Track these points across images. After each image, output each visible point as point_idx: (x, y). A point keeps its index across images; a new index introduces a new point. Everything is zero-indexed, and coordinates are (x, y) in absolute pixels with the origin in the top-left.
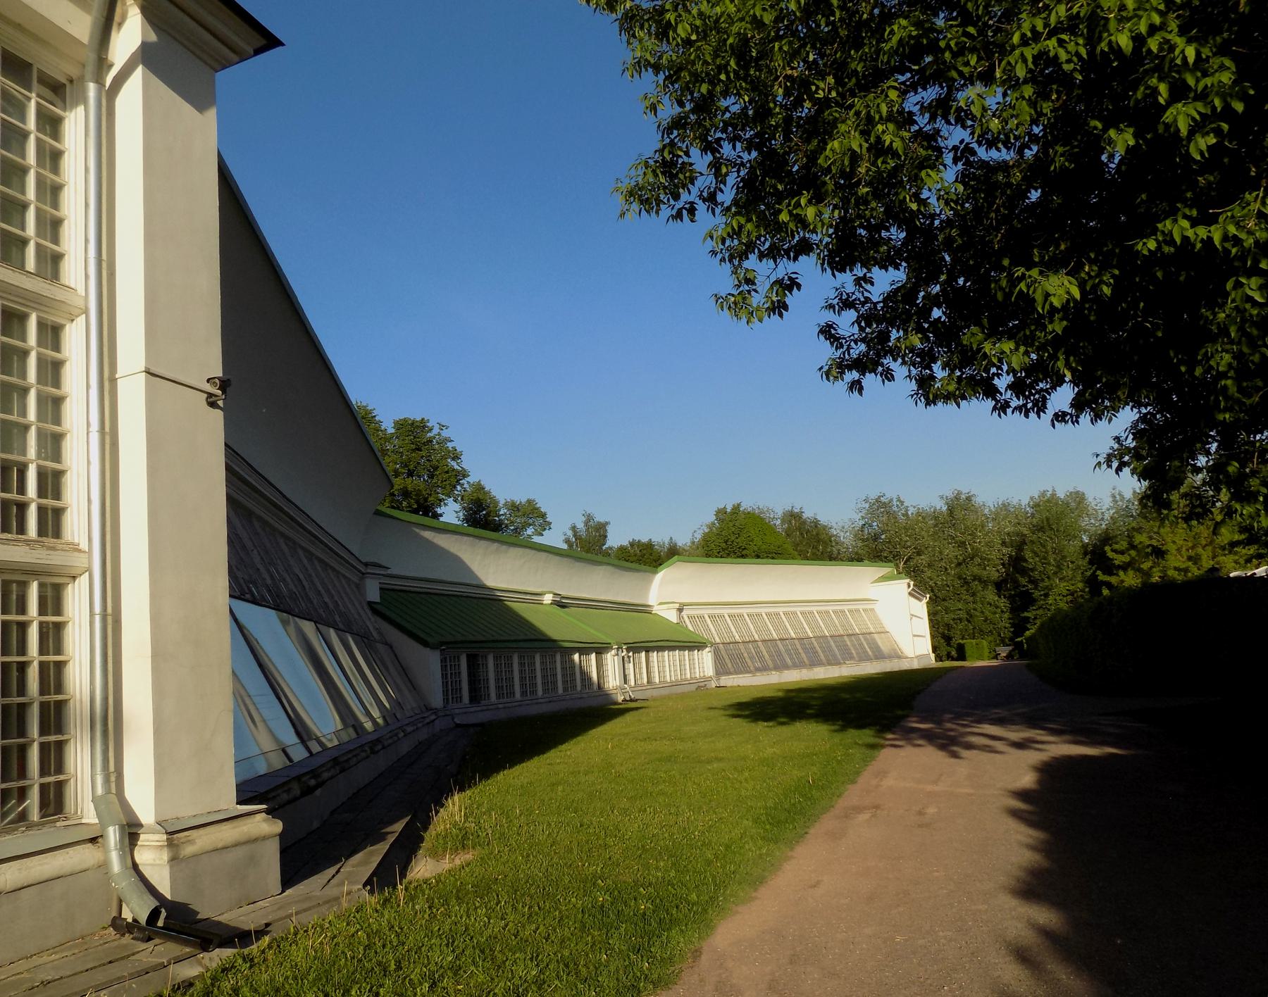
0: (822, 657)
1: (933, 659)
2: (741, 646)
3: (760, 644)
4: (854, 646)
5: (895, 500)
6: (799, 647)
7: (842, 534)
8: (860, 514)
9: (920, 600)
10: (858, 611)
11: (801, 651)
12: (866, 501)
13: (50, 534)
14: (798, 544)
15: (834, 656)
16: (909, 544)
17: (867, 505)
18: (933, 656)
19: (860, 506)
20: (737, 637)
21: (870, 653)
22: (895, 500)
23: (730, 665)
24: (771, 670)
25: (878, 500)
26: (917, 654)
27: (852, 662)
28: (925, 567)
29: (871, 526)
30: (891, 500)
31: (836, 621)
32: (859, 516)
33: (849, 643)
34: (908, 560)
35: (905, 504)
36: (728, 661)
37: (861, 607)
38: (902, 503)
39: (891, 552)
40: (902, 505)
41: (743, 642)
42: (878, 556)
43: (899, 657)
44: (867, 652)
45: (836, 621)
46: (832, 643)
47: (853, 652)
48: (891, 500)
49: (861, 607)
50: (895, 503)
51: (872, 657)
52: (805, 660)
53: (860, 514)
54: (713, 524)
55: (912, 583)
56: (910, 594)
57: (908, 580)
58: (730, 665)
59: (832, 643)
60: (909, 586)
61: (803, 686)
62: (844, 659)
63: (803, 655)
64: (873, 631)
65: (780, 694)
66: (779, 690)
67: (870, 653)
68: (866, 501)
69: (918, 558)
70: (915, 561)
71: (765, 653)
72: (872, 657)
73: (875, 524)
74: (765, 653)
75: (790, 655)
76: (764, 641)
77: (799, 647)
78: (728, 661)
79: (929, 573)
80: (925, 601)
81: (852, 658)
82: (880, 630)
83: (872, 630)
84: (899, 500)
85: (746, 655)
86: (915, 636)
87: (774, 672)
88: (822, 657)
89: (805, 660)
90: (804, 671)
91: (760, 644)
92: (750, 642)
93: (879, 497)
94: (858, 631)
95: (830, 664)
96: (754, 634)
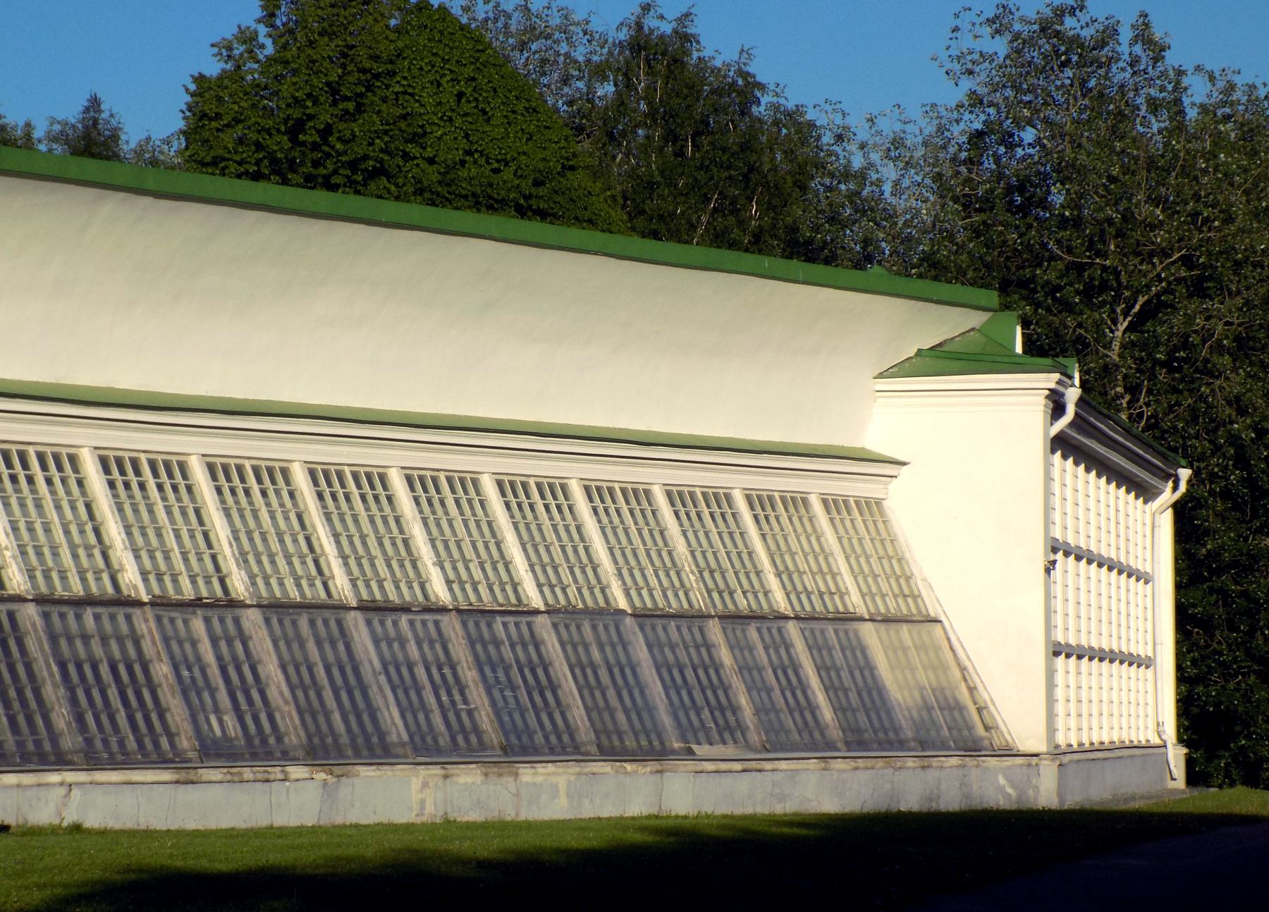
0: (578, 715)
1: (1179, 770)
2: (145, 624)
3: (252, 619)
4: (747, 669)
5: (1126, 34)
6: (460, 651)
7: (889, 172)
8: (967, 84)
9: (1145, 492)
10: (797, 502)
11: (469, 675)
12: (998, 24)
13: (1069, 431)
14: (651, 186)
15: (641, 710)
16: (1160, 237)
17: (1000, 47)
18: (1176, 756)
19: (966, 42)
20: (130, 577)
21: (827, 714)
22: (1126, 34)
23: (62, 717)
24: (287, 757)
25: (1046, 28)
26: (1067, 736)
27: (729, 750)
28: (1219, 348)
29: (1009, 141)
30: (1109, 34)
31: (681, 547)
32: (958, 93)
33: (725, 656)
34: (1149, 312)
35: (1172, 59)
36: (53, 693)
37: (815, 487)
38: (1158, 51)
39: (1080, 268)
40: (1156, 60)
41: (160, 603)
42: (1023, 284)
43: (972, 747)
44: (813, 709)
45: (681, 547)
46: (641, 653)
47: (743, 700)
48: (1109, 34)
49: (815, 487)
50: (1124, 49)
51: (835, 733)
52: (485, 719)
53: (967, 84)
54: (247, 38)
55: (1073, 394)
56: (1060, 444)
57: (1050, 380)
58: (62, 717)
59: (641, 653)
60: (1057, 409)
61: (273, 857)
62: (692, 733)
63: (478, 696)
64: (862, 611)
65: (648, 838)
66: (643, 829)
67: (827, 714)
68: (998, 24)
69: (1193, 305)
70: (1177, 320)
71: (271, 669)
72: (835, 733)
73: (1029, 135)
74: (271, 669)
75: (404, 687)
76: (275, 608)
77: (460, 651)
78: (53, 693)
79: (1235, 381)
80: (1168, 496)
81: (729, 730)
82: (893, 606)
83: (856, 602)
84: (1143, 34)
85: (162, 670)
86: (1057, 650)
87: (297, 772)
88: (578, 715)
89: (485, 719)
90: (468, 777)
91: (252, 619)
92: (197, 603)
93: (1060, 13)
94: (780, 602)
95: (611, 751)
96: (230, 564)
